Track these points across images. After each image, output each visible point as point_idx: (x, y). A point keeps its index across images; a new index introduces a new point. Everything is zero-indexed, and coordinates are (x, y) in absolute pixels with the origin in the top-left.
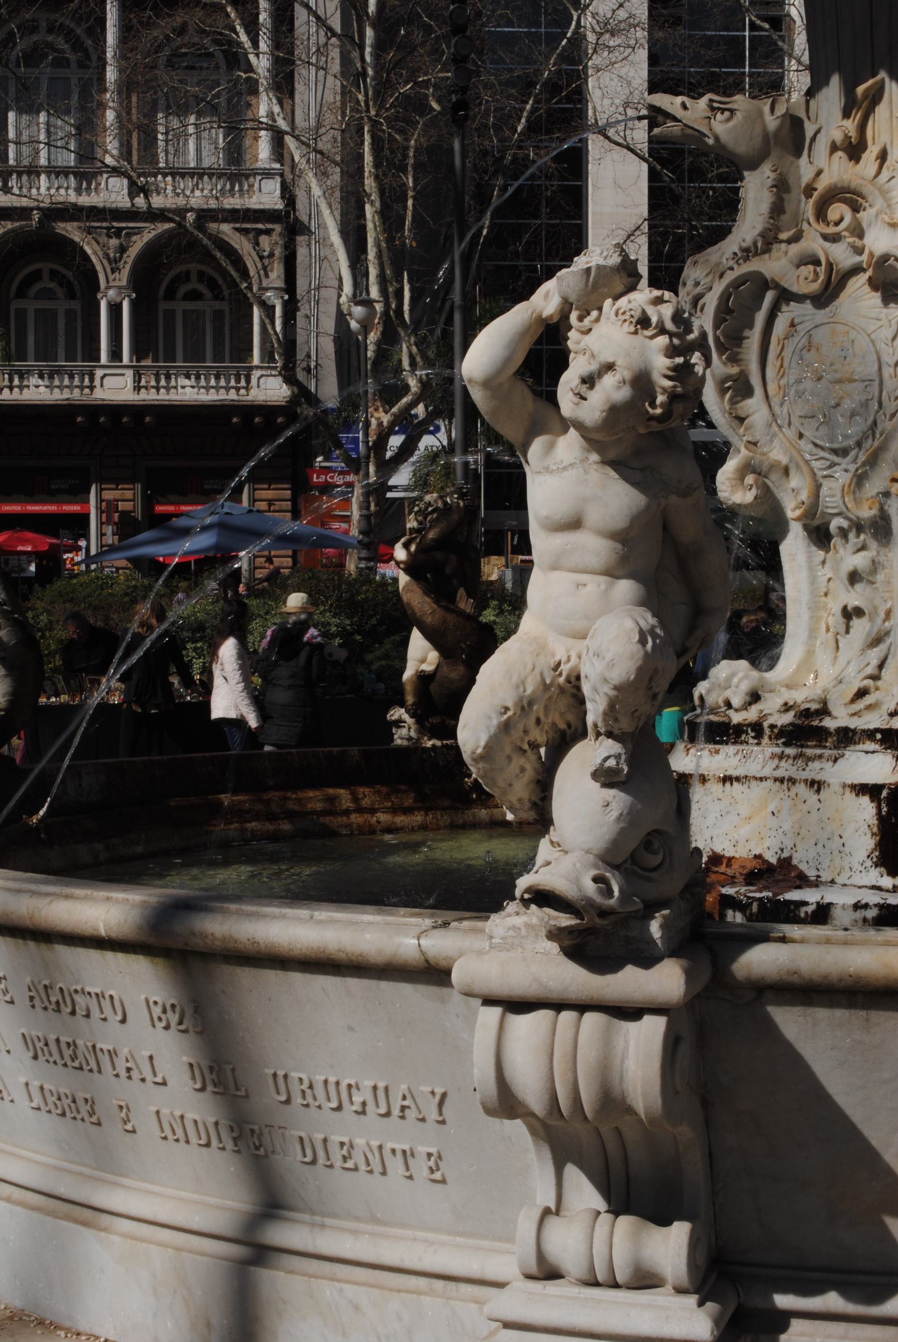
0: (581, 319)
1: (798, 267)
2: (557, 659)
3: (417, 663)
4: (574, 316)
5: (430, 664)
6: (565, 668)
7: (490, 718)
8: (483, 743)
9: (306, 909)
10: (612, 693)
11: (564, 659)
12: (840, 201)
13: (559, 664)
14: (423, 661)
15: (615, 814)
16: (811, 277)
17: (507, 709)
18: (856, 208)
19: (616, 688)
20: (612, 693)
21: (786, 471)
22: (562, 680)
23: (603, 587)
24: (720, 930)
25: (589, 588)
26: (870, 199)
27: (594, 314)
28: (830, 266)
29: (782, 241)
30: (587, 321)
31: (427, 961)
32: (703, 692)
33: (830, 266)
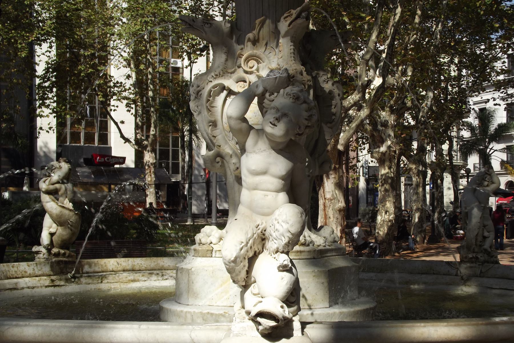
0: (270, 96)
1: (237, 83)
2: (258, 223)
3: (48, 228)
4: (267, 95)
5: (54, 228)
6: (261, 227)
7: (236, 246)
8: (234, 256)
9: (445, 322)
10: (291, 236)
11: (260, 224)
12: (254, 59)
13: (259, 225)
14: (50, 227)
15: (285, 282)
16: (243, 86)
17: (242, 242)
18: (258, 63)
19: (292, 234)
20: (291, 236)
21: (231, 156)
22: (260, 231)
23: (274, 196)
24: (64, 324)
25: (269, 197)
26: (263, 60)
27: (276, 94)
28: (250, 82)
29: (229, 73)
30: (272, 97)
31: (193, 340)
32: (201, 238)
33: (250, 82)
